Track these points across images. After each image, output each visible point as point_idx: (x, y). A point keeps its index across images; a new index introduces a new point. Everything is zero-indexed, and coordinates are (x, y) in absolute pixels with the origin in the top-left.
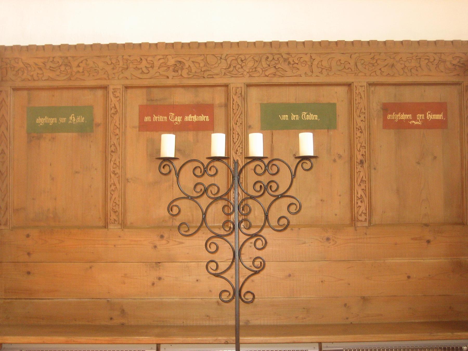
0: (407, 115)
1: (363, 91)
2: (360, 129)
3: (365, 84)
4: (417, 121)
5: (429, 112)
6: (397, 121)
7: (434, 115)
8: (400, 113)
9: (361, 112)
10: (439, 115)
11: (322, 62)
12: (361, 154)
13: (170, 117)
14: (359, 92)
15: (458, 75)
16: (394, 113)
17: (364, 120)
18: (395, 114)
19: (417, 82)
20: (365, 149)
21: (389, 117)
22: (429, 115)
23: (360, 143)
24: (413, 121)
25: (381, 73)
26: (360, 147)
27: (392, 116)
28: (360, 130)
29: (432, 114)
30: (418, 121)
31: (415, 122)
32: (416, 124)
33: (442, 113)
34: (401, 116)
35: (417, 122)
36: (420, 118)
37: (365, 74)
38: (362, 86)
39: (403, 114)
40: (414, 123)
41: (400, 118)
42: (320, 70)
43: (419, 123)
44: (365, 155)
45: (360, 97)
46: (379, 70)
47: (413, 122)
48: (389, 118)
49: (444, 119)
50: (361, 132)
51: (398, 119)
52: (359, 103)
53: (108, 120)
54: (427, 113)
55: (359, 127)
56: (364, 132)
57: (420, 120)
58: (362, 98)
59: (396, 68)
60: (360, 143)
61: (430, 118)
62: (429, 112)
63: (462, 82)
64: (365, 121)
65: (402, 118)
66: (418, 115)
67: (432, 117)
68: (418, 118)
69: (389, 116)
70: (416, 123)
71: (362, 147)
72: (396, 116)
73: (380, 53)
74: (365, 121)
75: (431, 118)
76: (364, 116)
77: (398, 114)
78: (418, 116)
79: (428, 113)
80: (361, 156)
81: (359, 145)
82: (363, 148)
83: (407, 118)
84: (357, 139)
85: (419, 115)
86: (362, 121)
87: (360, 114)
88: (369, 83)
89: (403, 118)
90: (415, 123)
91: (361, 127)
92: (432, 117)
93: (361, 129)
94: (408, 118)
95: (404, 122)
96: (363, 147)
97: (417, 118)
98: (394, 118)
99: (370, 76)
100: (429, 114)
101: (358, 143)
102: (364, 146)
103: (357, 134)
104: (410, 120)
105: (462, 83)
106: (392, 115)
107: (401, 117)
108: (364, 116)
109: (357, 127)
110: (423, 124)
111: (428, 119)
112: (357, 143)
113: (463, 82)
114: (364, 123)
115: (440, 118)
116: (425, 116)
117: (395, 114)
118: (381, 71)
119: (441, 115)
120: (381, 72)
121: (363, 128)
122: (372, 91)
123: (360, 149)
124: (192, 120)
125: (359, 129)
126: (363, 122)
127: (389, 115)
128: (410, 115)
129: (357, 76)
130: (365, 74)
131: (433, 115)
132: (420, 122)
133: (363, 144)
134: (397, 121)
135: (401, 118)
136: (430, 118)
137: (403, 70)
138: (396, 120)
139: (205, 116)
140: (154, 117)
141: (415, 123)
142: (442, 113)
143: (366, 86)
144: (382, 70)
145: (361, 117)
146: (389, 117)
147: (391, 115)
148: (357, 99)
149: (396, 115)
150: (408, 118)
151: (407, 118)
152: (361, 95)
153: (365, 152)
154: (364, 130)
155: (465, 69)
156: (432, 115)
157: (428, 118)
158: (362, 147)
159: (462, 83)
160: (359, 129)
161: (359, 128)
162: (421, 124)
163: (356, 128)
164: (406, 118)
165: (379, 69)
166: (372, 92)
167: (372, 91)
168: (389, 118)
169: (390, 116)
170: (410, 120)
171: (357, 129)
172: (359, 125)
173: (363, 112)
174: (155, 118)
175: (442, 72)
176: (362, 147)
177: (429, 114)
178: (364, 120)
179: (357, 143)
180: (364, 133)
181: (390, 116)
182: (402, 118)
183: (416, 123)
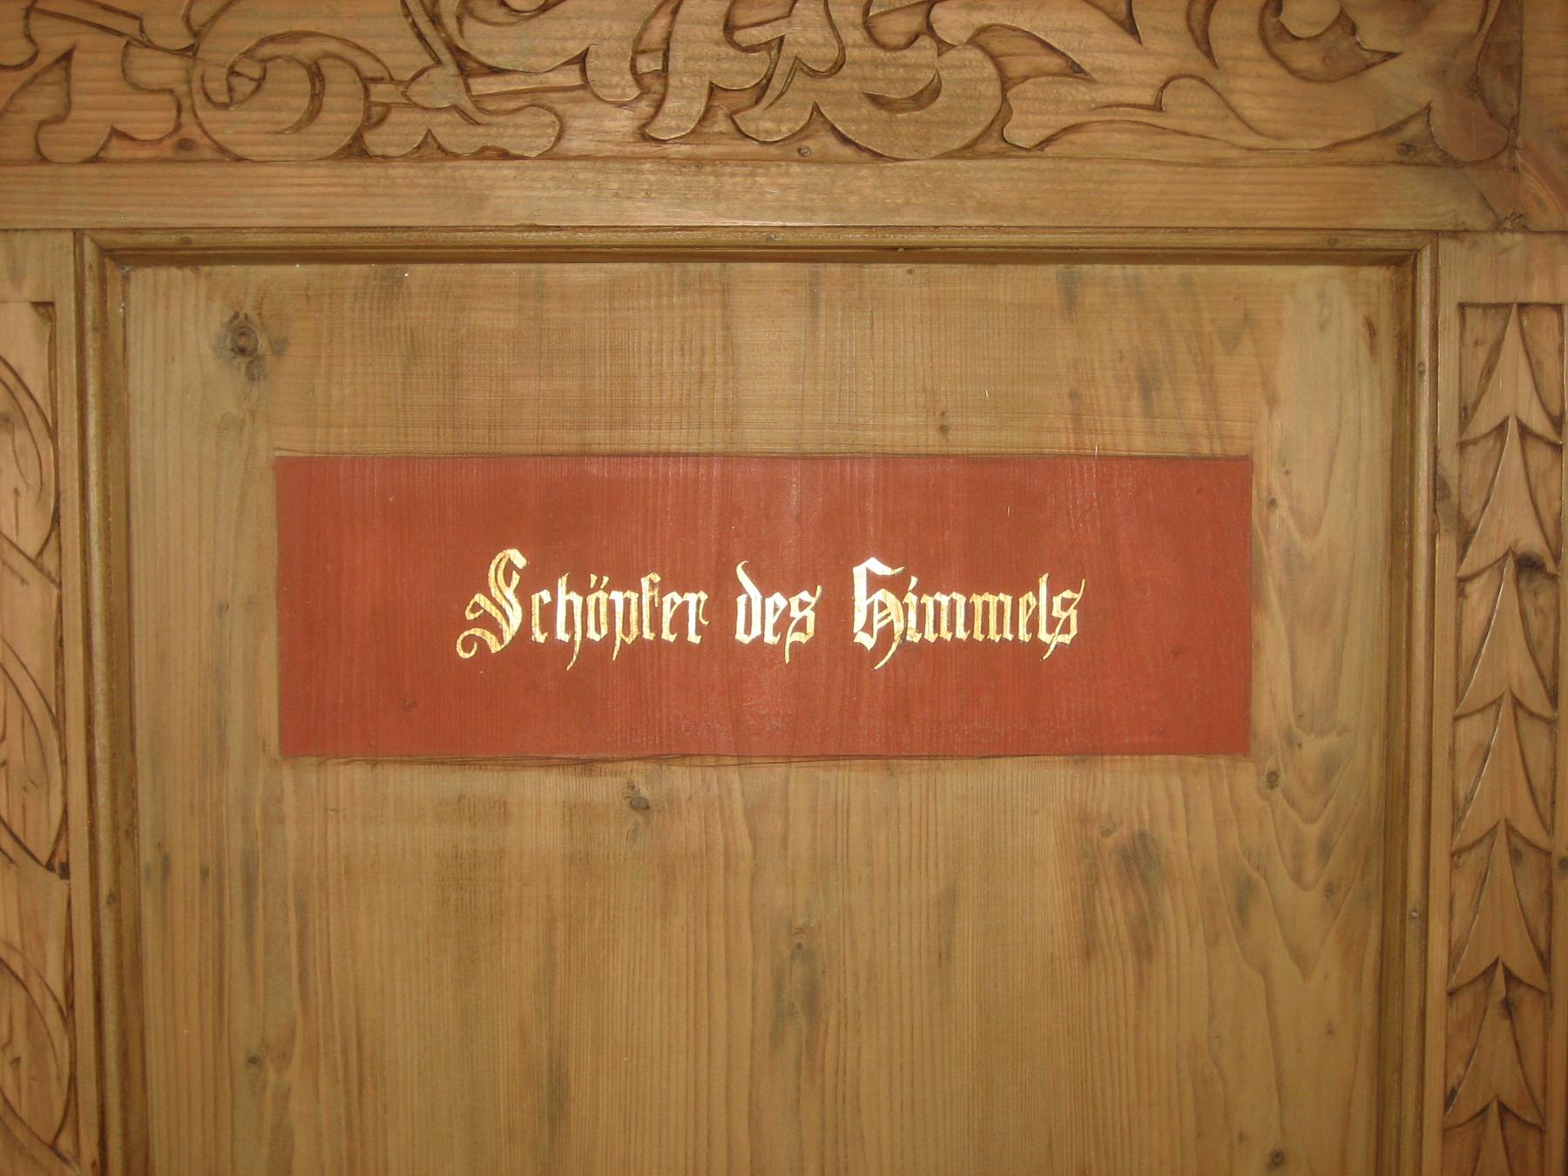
7: (993, 600)
8: (657, 578)
11: (67, 69)
13: (493, 567)
19: (1283, 250)
21: (482, 611)
29: (919, 591)
42: (742, 73)
53: (1236, 252)
59: (1431, 118)
63: (1408, 253)
67: (921, 627)
100: (875, 583)
111: (868, 641)
116: (836, 611)
131: (928, 600)
139: (778, 599)
140: (741, 600)
146: (482, 611)
157: (868, 628)
174: (571, 664)
177: (875, 583)
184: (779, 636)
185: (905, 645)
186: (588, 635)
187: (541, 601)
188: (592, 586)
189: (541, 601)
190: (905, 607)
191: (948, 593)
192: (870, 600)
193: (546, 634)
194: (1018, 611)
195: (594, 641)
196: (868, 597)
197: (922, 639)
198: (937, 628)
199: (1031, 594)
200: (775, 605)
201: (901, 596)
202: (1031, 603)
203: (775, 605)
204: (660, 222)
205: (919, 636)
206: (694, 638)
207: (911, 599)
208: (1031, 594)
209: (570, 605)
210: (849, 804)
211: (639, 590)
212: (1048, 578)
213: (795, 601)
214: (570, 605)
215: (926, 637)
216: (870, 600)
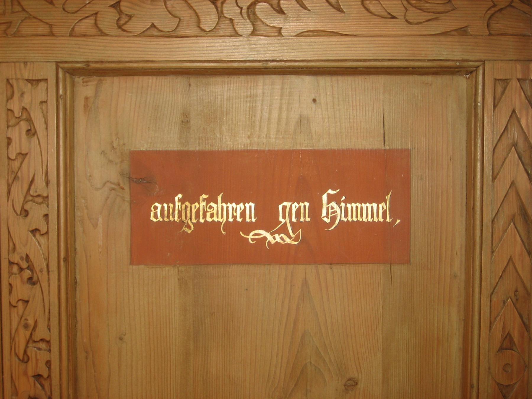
0: (234, 205)
1: (42, 102)
2: (28, 268)
3: (49, 72)
4: (279, 232)
5: (331, 192)
6: (189, 232)
7: (354, 205)
8: (204, 196)
9: (32, 192)
10: (375, 205)
12: (30, 373)
14: (24, 109)
15: (462, 32)
16: (180, 196)
17: (44, 230)
18: (182, 201)
20: (50, 351)
22: (333, 204)
23: (26, 326)
24: (260, 232)
25: (122, 22)
26: (28, 343)
27: (168, 207)
28: (27, 273)
29: (346, 202)
30: (283, 230)
31: (272, 234)
32: (273, 242)
33: (388, 197)
34: (211, 207)
35: (277, 236)
36: (294, 220)
37: (51, 26)
38: (39, 81)
39: (216, 203)
40: (265, 238)
41: (205, 216)
43: (288, 241)
44: (49, 376)
45: (28, 131)
46: (113, 10)
47: (264, 233)
48: (156, 216)
49: (394, 221)
50: (30, 279)
51: (194, 221)
52: (23, 155)
54: (325, 197)
55: (22, 258)
56: (43, 277)
57: (292, 224)
58: (35, 133)
60: (26, 326)
61: (333, 219)
62: (331, 192)
63: (477, 64)
64: (47, 233)
65: (212, 216)
66: (285, 204)
67: (346, 215)
68: (284, 217)
69: (156, 208)
70: (274, 238)
71: (35, 342)
72: (186, 207)
73: (71, 35)
74: (47, 233)
75: (340, 216)
76: (43, 210)
77: (195, 200)
78: (284, 208)
79: (329, 195)
80: (32, 380)
81: (23, 336)
82: (39, 349)
83: (234, 217)
84: (14, 311)
85: (287, 204)
86: (34, 231)
87: (25, 202)
88: (66, 65)
89: (221, 220)
90: (270, 238)
91: (31, 257)
92: (346, 215)
93: (31, 268)
94: (239, 219)
95: (223, 233)
96: (43, 345)
97: (281, 219)
98: (180, 216)
99: (72, 34)
100: (330, 198)
101: (17, 330)
102: (42, 340)
103: (14, 289)
104: (248, 227)
105: (478, 67)
106: (171, 205)
107: (208, 215)
108: (43, 210)
109: (16, 258)
110: (304, 241)
111: (327, 220)
112: (14, 326)
113: (483, 62)
114: (43, 240)
115: (378, 216)
117: (182, 201)
118: (120, 12)
119: (383, 204)
120: (119, 20)
121: (39, 263)
122: (87, 98)
123: (25, 352)
124: (381, 220)
125: (21, 269)
126: (38, 235)
127: (159, 206)
128: (247, 205)
129: (15, 35)
130: (51, 26)
131: (349, 206)
132: (290, 237)
133: (41, 332)
134: (189, 232)
135: (209, 219)
136: (333, 219)
137: (217, 8)
138: (189, 227)
141: (270, 238)
142: (388, 197)
143: (52, 81)
144: (123, 8)
145: (31, 213)
147: (165, 205)
148: (13, 138)
149: (187, 203)
150: (239, 219)
151: (234, 217)
152: (29, 120)
153: (48, 363)
154: (41, 271)
155: (494, 6)
156: (343, 205)
157: (327, 217)
158: (34, 345)
159: (478, 67)
160: (21, 269)
161: (24, 265)
162: (296, 243)
163: (11, 263)
164: (231, 220)
165: (112, 6)
166: (86, 106)
167: (87, 98)
168: (156, 216)
169: (163, 208)
170: (248, 227)
171: (15, 269)
172: (22, 250)
173: (39, 196)
175: (394, 17)
176: (35, 342)
177: (330, 198)
178: (44, 230)
179: (14, 326)
180: (45, 285)
181: (163, 208)
182: (212, 216)
183: (274, 238)
184: (233, 219)
185: (341, 221)
186: (306, 220)
187: (179, 198)
188: (342, 200)
189: (179, 198)
190: (341, 208)
191: (371, 203)
192: (328, 206)
193: (242, 218)
194: (282, 212)
195: (279, 219)
196: (327, 205)
197: (218, 221)
198: (352, 217)
199: (242, 204)
200: (240, 208)
201: (338, 204)
202: (384, 207)
203: (240, 208)
204: (255, 57)
205: (352, 219)
206: (388, 220)
207: (343, 205)
208: (242, 204)
209: (222, 207)
210: (49, 306)
211: (174, 204)
212: (222, 195)
213: (238, 206)
214: (222, 207)
215: (358, 219)
216: (328, 206)
